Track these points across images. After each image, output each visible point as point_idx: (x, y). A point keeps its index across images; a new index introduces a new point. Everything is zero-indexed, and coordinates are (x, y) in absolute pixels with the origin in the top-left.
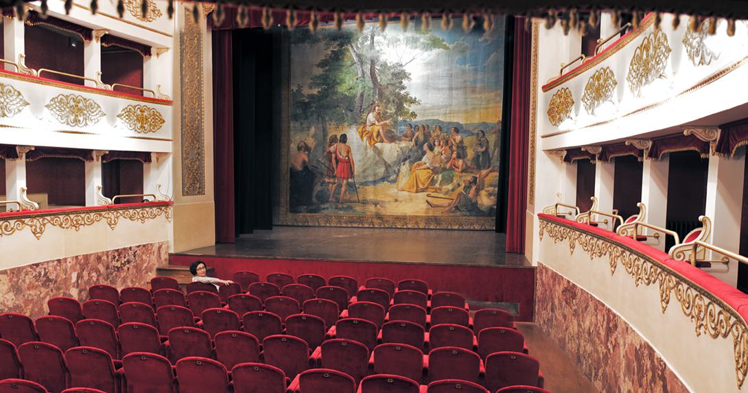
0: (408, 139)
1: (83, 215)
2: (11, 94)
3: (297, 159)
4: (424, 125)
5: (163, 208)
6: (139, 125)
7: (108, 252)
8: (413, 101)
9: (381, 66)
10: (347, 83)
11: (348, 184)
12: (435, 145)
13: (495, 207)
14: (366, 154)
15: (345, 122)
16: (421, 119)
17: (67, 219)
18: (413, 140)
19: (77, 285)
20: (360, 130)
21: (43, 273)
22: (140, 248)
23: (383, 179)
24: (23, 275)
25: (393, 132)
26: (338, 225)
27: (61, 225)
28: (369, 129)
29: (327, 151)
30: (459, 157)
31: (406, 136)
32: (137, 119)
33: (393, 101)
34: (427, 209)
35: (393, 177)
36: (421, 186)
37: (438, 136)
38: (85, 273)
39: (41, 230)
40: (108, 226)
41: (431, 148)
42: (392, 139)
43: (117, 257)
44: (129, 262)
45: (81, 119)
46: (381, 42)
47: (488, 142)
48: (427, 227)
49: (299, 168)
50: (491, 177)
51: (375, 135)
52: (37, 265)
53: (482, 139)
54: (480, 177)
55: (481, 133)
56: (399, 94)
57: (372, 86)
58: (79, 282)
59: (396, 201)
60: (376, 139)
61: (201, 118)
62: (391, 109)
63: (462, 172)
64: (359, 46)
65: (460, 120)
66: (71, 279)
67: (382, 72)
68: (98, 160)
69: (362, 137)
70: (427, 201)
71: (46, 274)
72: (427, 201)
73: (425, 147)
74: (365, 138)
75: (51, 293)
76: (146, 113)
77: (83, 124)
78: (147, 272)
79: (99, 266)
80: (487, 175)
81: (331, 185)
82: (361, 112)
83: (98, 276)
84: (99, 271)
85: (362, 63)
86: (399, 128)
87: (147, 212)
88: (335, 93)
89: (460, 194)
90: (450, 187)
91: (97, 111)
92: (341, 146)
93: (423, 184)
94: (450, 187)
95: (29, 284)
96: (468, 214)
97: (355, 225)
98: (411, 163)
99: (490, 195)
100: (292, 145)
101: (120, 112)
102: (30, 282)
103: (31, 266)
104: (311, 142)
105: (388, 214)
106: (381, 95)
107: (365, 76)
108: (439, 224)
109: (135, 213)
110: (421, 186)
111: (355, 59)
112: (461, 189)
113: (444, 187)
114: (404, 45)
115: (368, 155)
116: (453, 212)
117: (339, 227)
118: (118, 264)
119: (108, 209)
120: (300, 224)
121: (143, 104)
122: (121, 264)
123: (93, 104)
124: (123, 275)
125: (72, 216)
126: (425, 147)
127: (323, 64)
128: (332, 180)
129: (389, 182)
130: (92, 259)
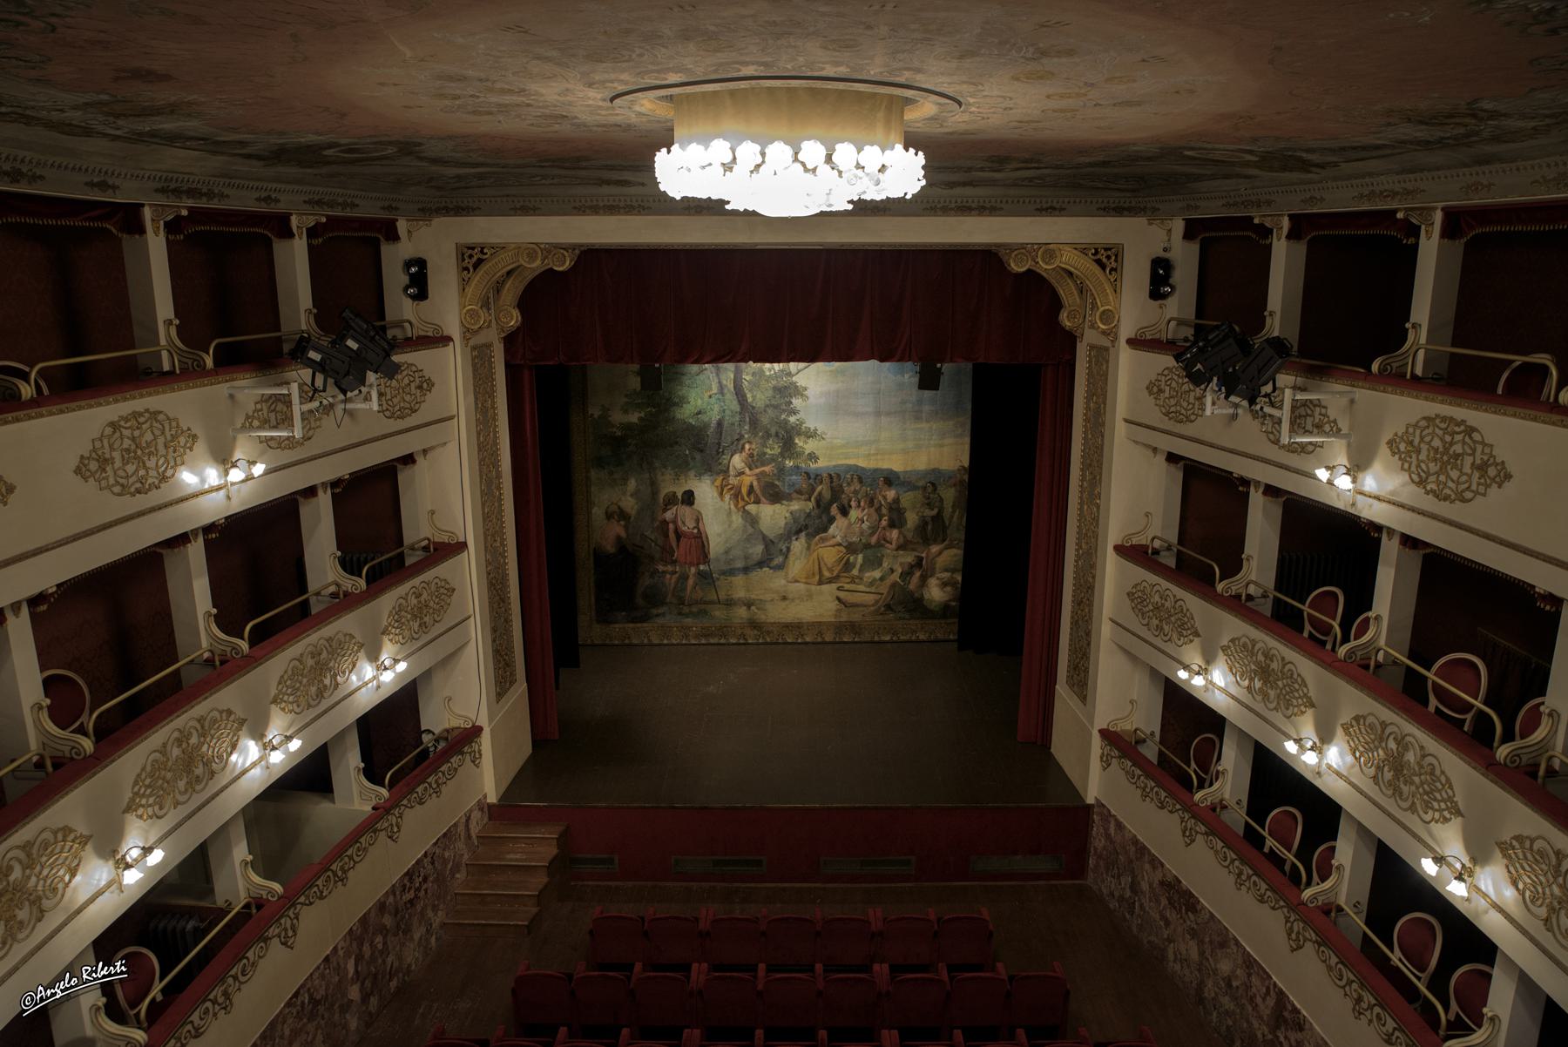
3: (608, 534)
4: (832, 473)
5: (466, 749)
7: (393, 886)
8: (811, 435)
12: (851, 507)
15: (690, 469)
18: (812, 499)
20: (718, 483)
25: (777, 486)
28: (733, 481)
29: (660, 519)
30: (892, 525)
31: (799, 492)
33: (777, 435)
35: (779, 560)
36: (827, 574)
37: (856, 492)
38: (366, 949)
39: (294, 931)
41: (844, 512)
42: (776, 497)
44: (425, 879)
47: (941, 500)
49: (610, 548)
50: (947, 556)
51: (744, 491)
52: (296, 995)
54: (927, 556)
55: (930, 483)
56: (786, 422)
57: (738, 410)
59: (784, 598)
65: (896, 464)
69: (721, 494)
70: (838, 599)
72: (838, 599)
73: (834, 510)
74: (727, 497)
80: (940, 553)
81: (668, 576)
82: (718, 453)
89: (894, 585)
90: (877, 574)
93: (830, 570)
94: (877, 574)
96: (907, 616)
97: (712, 641)
98: (810, 536)
99: (944, 584)
102: (291, 1030)
103: (288, 1004)
104: (629, 504)
105: (768, 621)
107: (726, 391)
110: (827, 574)
112: (895, 577)
113: (867, 575)
116: (881, 614)
117: (685, 644)
119: (381, 811)
121: (416, 581)
126: (834, 510)
128: (670, 568)
129: (771, 568)
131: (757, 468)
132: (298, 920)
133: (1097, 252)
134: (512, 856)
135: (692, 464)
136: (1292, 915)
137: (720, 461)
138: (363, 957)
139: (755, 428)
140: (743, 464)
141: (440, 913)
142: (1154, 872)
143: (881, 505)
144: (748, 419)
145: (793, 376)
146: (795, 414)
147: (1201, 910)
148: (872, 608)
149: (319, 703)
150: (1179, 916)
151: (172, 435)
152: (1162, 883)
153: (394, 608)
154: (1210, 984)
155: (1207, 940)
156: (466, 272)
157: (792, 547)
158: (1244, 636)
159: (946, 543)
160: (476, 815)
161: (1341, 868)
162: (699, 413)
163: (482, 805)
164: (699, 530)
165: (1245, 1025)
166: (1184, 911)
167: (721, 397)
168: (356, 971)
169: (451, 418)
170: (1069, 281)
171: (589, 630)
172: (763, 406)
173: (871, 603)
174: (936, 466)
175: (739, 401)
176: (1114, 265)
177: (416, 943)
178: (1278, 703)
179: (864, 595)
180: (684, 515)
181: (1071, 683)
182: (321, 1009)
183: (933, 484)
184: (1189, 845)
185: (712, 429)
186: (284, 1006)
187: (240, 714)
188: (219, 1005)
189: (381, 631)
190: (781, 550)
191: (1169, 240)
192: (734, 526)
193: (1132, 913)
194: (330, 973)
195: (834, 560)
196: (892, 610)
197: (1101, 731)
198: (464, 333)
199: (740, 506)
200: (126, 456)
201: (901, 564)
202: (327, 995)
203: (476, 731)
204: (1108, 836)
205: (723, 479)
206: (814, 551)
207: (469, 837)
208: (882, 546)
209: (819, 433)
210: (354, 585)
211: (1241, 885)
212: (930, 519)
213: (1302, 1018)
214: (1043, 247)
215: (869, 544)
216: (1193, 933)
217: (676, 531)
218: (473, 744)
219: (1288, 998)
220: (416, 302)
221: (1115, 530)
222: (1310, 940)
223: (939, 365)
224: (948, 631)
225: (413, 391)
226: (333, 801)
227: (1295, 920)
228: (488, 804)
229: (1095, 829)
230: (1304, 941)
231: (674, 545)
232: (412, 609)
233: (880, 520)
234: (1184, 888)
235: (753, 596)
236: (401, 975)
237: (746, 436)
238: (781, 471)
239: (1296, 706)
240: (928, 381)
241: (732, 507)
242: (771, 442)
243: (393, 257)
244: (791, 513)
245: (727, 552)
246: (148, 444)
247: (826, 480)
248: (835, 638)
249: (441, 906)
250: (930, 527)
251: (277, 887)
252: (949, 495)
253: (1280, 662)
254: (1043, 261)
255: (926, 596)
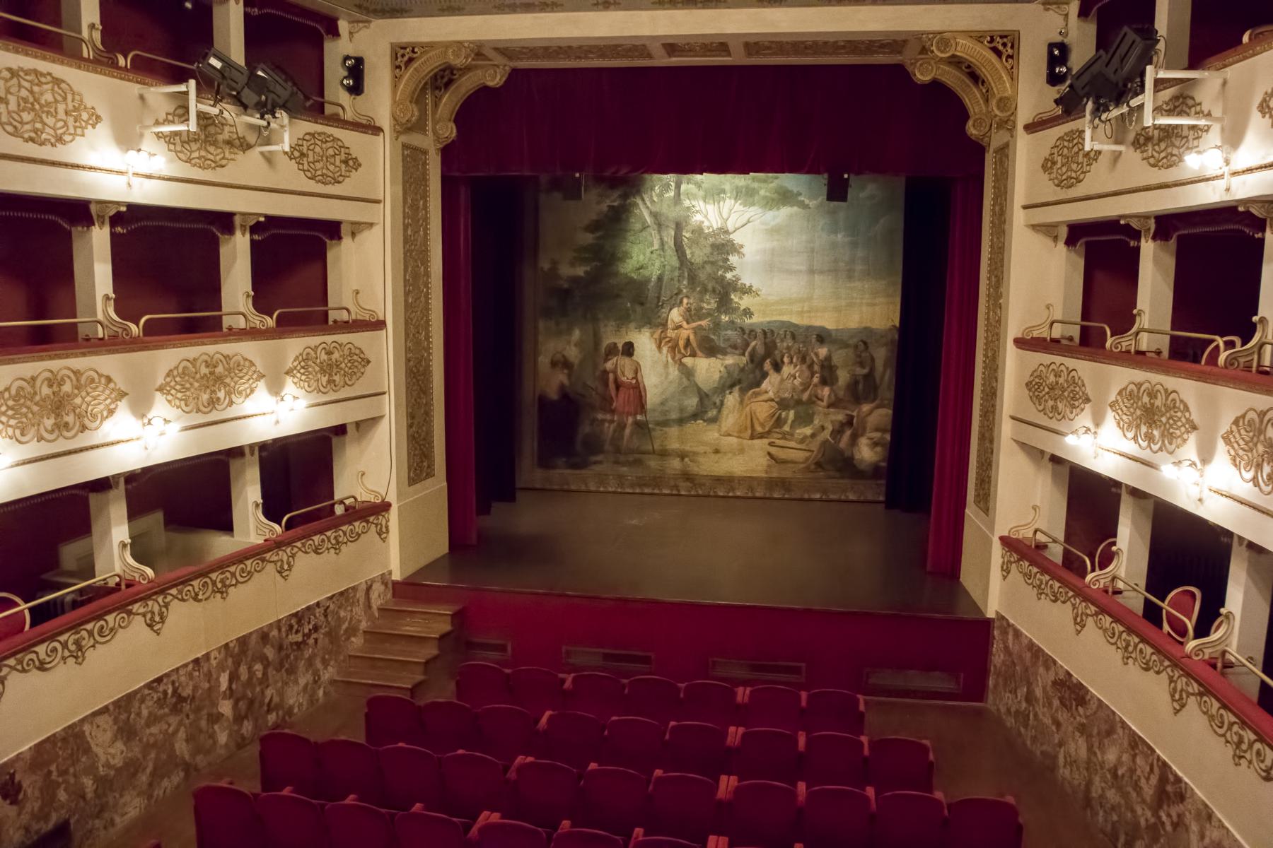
0: (737, 352)
1: (232, 569)
2: (94, 385)
3: (552, 382)
4: (766, 329)
5: (371, 519)
6: (324, 380)
7: (279, 621)
8: (746, 291)
9: (693, 232)
10: (635, 258)
11: (638, 424)
12: (783, 362)
13: (883, 464)
14: (667, 374)
15: (631, 322)
16: (761, 320)
17: (206, 582)
18: (747, 354)
19: (230, 693)
20: (656, 335)
21: (170, 691)
22: (334, 599)
23: (695, 416)
24: (136, 704)
25: (712, 340)
26: (619, 490)
27: (196, 599)
28: (671, 333)
29: (601, 368)
30: (824, 382)
31: (734, 347)
32: (321, 369)
33: (714, 291)
34: (769, 466)
35: (712, 413)
36: (759, 429)
37: (788, 348)
38: (243, 670)
39: (161, 618)
40: (278, 575)
41: (777, 367)
42: (711, 350)
43: (296, 627)
44: (316, 628)
45: (221, 394)
46: (692, 194)
47: (873, 359)
48: (768, 495)
49: (553, 394)
50: (877, 415)
51: (681, 343)
52: (159, 680)
53: (863, 355)
54: (858, 416)
55: (862, 342)
56: (723, 278)
57: (678, 265)
58: (234, 686)
59: (717, 451)
60: (683, 351)
61: (430, 354)
62: (709, 303)
63: (829, 407)
64: (655, 199)
65: (827, 322)
66: (219, 686)
67: (694, 242)
68: (252, 454)
69: (659, 347)
70: (769, 454)
71: (175, 691)
72: (769, 454)
73: (767, 365)
74: (665, 350)
75: (187, 721)
76: (336, 355)
77: (199, 361)
78: (348, 639)
79: (265, 650)
80: (871, 412)
81: (607, 425)
82: (657, 306)
83: (265, 668)
84: (267, 658)
85: (660, 226)
86: (723, 333)
87: (345, 534)
88: (616, 274)
89: (825, 442)
90: (808, 431)
91: (250, 373)
92: (625, 361)
93: (762, 425)
94: (808, 431)
95: (149, 717)
96: (837, 475)
97: (646, 491)
98: (743, 391)
99: (875, 444)
100: (541, 359)
101: (290, 365)
102: (150, 713)
103: (149, 686)
104: (573, 353)
105: (701, 473)
106: (693, 279)
107: (666, 247)
108: (788, 490)
109: (323, 541)
110: (759, 429)
111: (649, 219)
112: (826, 435)
113: (798, 431)
114: (733, 201)
115: (671, 377)
116: (812, 472)
117: (621, 493)
118: (299, 638)
119: (275, 545)
120: (556, 487)
121: (329, 339)
122: (304, 635)
123: (242, 363)
124: (308, 653)
125: (214, 576)
126: (767, 365)
127: (594, 227)
128: (608, 417)
129: (704, 421)
130: (254, 639)
131: (694, 322)
132: (167, 610)
133: (992, 40)
134: (407, 628)
135: (632, 317)
136: (1176, 672)
137: (659, 314)
138: (238, 678)
139: (693, 283)
140: (681, 318)
141: (330, 669)
142: (1048, 674)
143: (813, 361)
144: (686, 274)
145: (730, 234)
146: (731, 270)
147: (1089, 700)
148: (802, 466)
149: (210, 411)
150: (1069, 715)
151: (74, 106)
152: (1055, 683)
153: (301, 354)
154: (1097, 779)
155: (1095, 731)
156: (398, 70)
157: (726, 400)
158: (1130, 383)
159: (877, 402)
160: (378, 588)
161: (1231, 617)
162: (641, 268)
163: (384, 579)
164: (637, 381)
165: (1129, 815)
166: (1074, 707)
167: (662, 253)
168: (230, 687)
169: (378, 202)
170: (975, 90)
171: (529, 472)
172: (701, 262)
173: (801, 460)
174: (869, 325)
175: (679, 257)
176: (1010, 51)
177: (301, 688)
178: (1163, 441)
179: (795, 453)
180: (624, 366)
181: (977, 502)
182: (186, 707)
183: (865, 343)
184: (1080, 632)
185: (652, 284)
186: (144, 686)
187: (121, 385)
188: (69, 651)
189: (285, 371)
190: (715, 403)
191: (1067, 25)
192: (671, 377)
193: (1026, 726)
194: (199, 677)
195: (767, 414)
196: (823, 468)
197: (1002, 539)
198: (394, 126)
199: (677, 358)
200: (22, 104)
201: (832, 422)
202: (194, 697)
203: (385, 507)
204: (1006, 647)
205: (662, 332)
206: (747, 405)
207: (368, 605)
208: (814, 403)
209: (754, 289)
210: (262, 321)
211: (1127, 659)
212: (861, 377)
213: (1183, 785)
214: (938, 37)
215: (801, 400)
216: (1082, 729)
217: (616, 380)
218: (381, 517)
219: (1170, 768)
220: (353, 97)
221: (1013, 330)
222: (1193, 694)
223: (846, 176)
224: (875, 491)
225: (338, 163)
226: (233, 536)
227: (1179, 677)
228: (393, 581)
229: (995, 646)
230: (1188, 697)
231: (613, 393)
232: (321, 363)
233: (812, 377)
234: (1075, 681)
235: (687, 448)
236: (281, 713)
237: (685, 291)
238: (717, 325)
239: (1179, 437)
240: (837, 192)
241: (670, 359)
242: (708, 297)
243: (336, 52)
244: (726, 367)
245: (662, 404)
246: (48, 104)
247: (760, 335)
248: (765, 494)
249: (332, 663)
250: (861, 386)
251: (149, 572)
252: (881, 355)
253: (1163, 394)
254: (939, 49)
255: (857, 456)
